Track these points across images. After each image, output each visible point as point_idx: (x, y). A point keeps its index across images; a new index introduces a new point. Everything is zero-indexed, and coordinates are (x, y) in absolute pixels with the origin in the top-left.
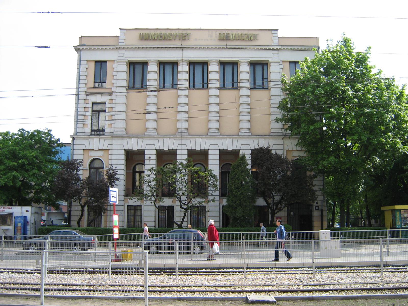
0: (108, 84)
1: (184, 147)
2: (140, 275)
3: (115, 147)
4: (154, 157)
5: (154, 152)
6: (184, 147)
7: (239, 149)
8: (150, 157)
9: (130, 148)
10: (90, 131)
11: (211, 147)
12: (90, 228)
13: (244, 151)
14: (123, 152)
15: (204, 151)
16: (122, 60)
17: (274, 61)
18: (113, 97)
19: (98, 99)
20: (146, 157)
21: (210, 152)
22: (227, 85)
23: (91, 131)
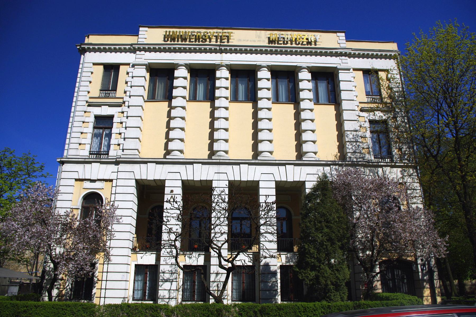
0: (119, 93)
1: (223, 177)
2: (398, 68)
3: (121, 175)
4: (179, 191)
5: (179, 184)
6: (223, 177)
7: (258, 180)
8: (172, 191)
9: (144, 177)
10: (87, 154)
11: (216, 177)
12: (61, 303)
13: (268, 260)
14: (133, 183)
15: (199, 185)
16: (141, 63)
17: (343, 67)
18: (124, 108)
19: (105, 111)
20: (167, 190)
21: (261, 184)
22: (280, 100)
23: (90, 154)
